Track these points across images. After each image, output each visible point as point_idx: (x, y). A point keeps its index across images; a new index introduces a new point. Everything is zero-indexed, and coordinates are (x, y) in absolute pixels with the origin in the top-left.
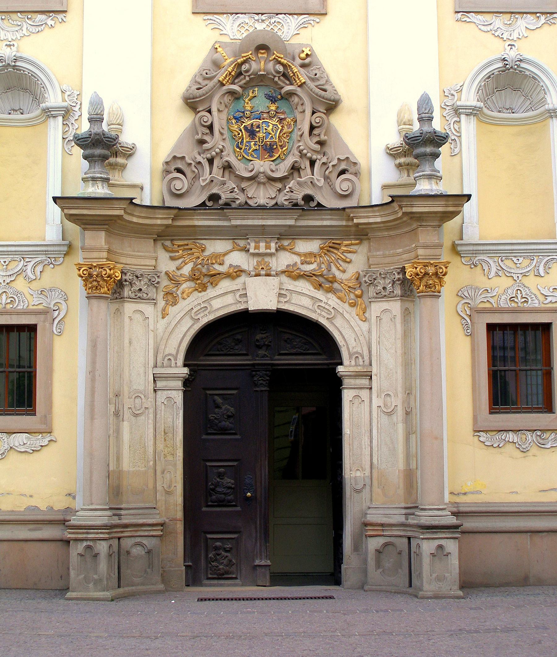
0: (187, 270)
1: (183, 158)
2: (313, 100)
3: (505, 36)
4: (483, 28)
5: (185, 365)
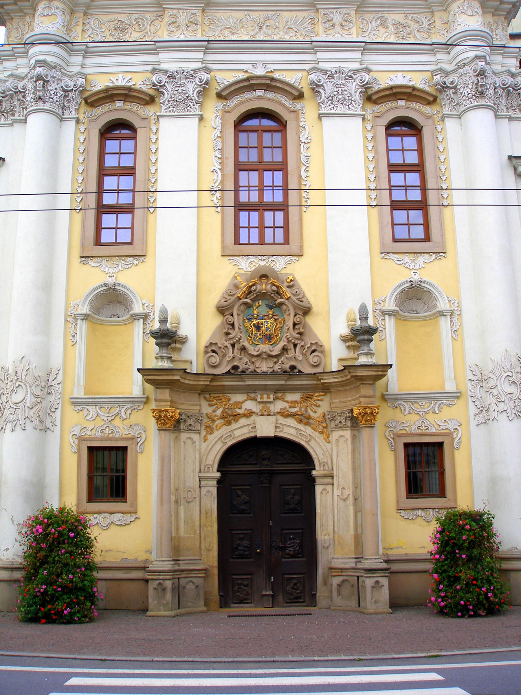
0: (219, 412)
3: (411, 268)
4: (399, 263)
5: (218, 471)
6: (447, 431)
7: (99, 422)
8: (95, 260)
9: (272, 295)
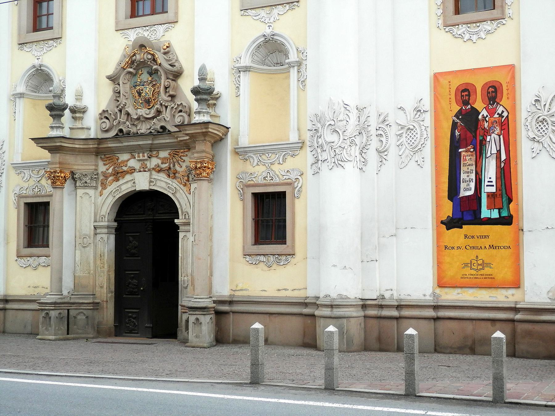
0: (110, 171)
1: (107, 111)
2: (166, 73)
3: (266, 22)
4: (255, 18)
5: (115, 221)
6: (289, 181)
7: (32, 183)
8: (28, 45)
9: (149, 63)
